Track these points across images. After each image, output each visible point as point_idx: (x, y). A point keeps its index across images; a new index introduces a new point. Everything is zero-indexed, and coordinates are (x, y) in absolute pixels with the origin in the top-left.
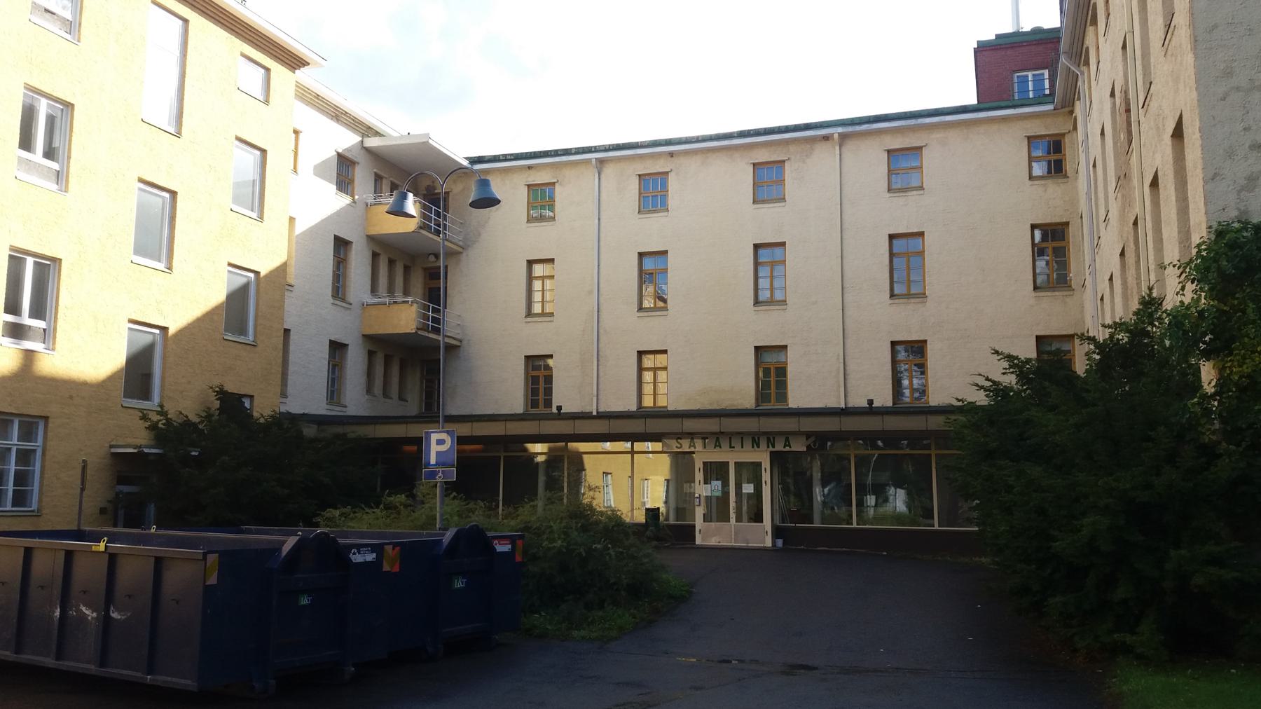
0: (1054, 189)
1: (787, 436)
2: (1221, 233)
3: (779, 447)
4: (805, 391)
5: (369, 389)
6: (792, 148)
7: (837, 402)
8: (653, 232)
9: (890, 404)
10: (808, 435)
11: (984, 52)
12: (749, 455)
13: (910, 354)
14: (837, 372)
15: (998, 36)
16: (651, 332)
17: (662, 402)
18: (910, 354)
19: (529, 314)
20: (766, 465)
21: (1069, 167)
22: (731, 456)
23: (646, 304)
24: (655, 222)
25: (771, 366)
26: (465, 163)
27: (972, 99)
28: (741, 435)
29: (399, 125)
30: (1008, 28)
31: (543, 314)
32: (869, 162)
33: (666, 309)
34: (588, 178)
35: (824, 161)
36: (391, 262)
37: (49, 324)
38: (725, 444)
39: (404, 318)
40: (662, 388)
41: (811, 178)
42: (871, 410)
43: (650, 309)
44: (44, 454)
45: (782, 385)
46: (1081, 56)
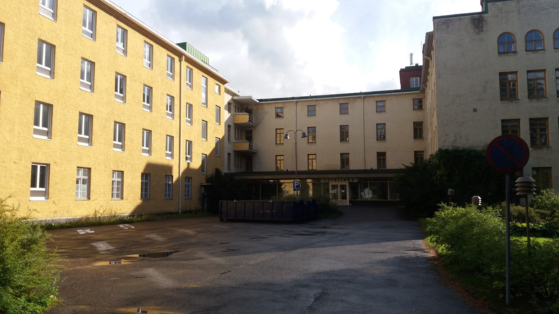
0: (419, 113)
1: (353, 179)
2: (440, 150)
3: (351, 181)
4: (353, 166)
5: (235, 166)
6: (350, 100)
7: (362, 167)
8: (311, 122)
9: (375, 167)
10: (358, 178)
11: (402, 72)
12: (343, 183)
13: (381, 156)
14: (363, 159)
15: (406, 67)
16: (312, 149)
17: (314, 168)
18: (381, 156)
19: (276, 144)
20: (348, 185)
21: (423, 107)
22: (339, 183)
23: (310, 141)
24: (312, 119)
25: (345, 159)
26: (258, 102)
27: (399, 87)
28: (341, 178)
29: (243, 93)
30: (409, 65)
31: (280, 144)
32: (371, 104)
33: (315, 143)
34: (293, 106)
35: (359, 103)
36: (238, 129)
37: (49, 129)
38: (337, 181)
39: (245, 146)
40: (314, 164)
41: (355, 108)
42: (372, 171)
43: (310, 143)
44: (150, 183)
45: (348, 164)
46: (427, 73)
